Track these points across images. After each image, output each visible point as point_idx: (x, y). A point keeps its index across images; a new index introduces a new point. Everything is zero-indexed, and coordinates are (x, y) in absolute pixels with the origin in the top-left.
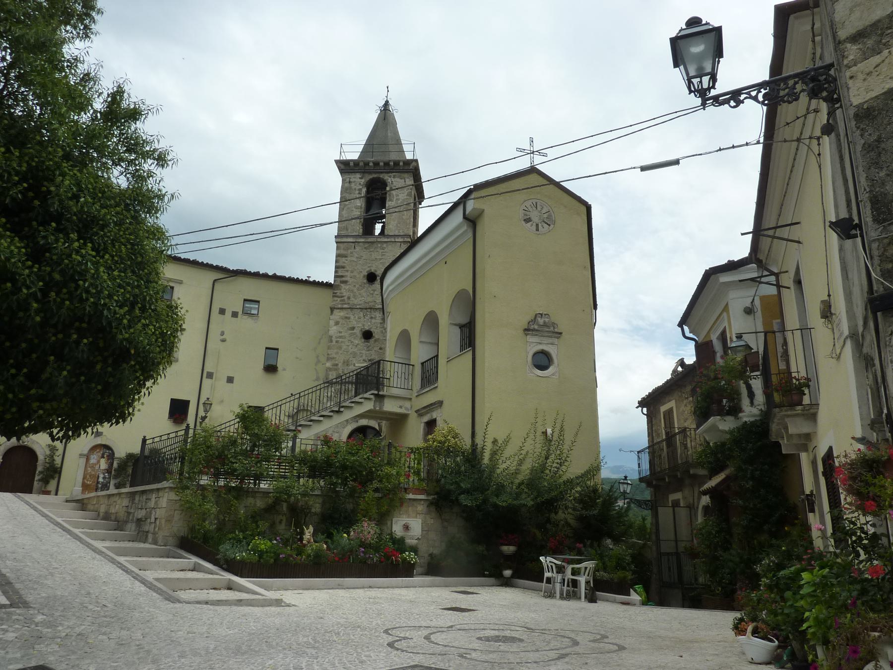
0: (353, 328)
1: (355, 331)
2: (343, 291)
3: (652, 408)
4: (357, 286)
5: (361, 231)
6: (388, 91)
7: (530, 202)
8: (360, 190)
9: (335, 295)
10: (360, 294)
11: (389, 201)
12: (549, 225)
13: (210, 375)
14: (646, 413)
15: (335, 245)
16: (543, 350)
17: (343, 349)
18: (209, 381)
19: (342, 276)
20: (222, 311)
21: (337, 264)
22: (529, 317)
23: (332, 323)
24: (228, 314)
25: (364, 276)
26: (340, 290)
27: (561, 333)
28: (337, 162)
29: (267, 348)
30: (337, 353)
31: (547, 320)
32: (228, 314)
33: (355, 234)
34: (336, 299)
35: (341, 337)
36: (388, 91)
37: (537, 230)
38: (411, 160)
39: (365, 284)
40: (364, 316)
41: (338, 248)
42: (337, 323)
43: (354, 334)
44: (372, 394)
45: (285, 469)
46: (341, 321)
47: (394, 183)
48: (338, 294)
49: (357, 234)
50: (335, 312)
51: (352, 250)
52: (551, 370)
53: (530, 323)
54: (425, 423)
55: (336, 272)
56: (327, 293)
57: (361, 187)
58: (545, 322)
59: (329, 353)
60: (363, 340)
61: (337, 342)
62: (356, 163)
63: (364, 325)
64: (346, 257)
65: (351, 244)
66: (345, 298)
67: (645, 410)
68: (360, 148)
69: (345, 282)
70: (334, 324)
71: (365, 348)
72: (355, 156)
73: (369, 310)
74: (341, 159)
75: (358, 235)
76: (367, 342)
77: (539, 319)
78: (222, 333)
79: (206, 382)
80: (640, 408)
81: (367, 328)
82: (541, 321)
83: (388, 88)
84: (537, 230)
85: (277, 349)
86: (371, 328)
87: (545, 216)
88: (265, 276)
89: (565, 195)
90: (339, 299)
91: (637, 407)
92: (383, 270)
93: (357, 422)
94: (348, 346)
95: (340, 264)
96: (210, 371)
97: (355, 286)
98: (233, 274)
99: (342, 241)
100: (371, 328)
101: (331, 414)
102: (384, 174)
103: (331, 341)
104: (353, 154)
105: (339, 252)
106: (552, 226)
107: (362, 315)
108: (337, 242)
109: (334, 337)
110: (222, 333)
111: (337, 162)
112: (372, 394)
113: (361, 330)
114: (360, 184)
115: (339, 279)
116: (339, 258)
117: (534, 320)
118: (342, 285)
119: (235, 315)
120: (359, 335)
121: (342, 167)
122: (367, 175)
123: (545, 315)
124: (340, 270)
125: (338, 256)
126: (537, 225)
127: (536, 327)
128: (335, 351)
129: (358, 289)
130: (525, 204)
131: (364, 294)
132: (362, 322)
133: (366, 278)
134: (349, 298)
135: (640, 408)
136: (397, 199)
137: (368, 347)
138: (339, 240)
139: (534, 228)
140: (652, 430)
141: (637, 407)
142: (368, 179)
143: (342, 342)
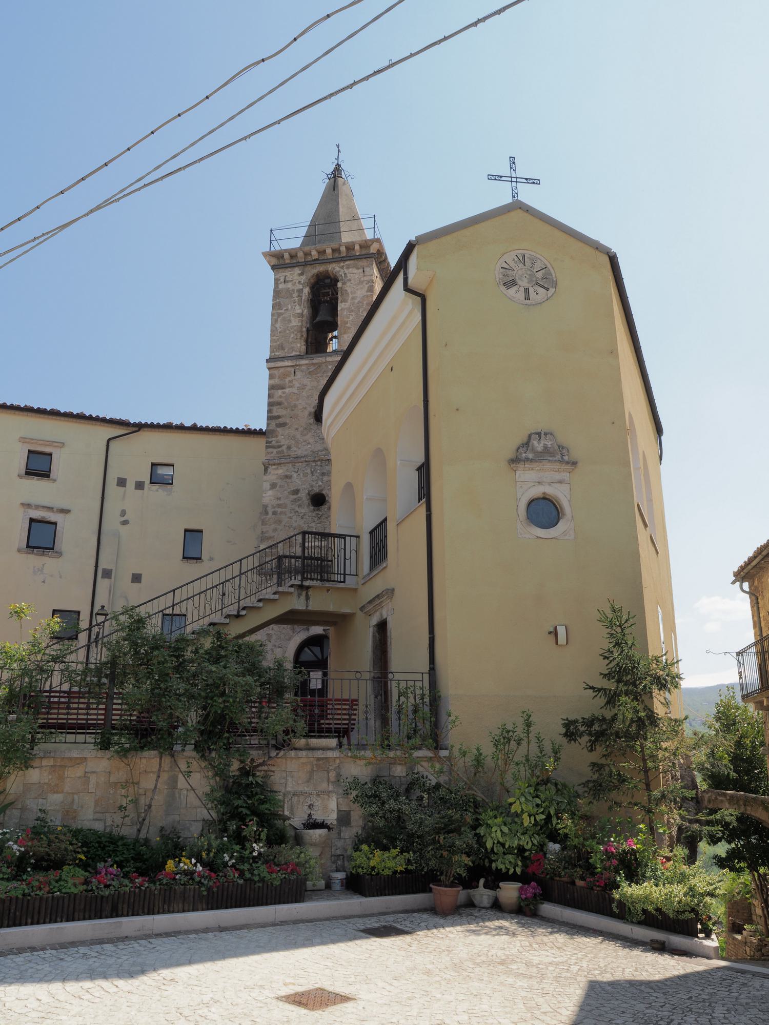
0: (296, 492)
1: (299, 495)
2: (280, 438)
3: (756, 583)
4: (301, 429)
5: (304, 347)
6: (339, 151)
7: (513, 254)
8: (300, 291)
9: (269, 446)
10: (305, 441)
11: (341, 302)
12: (547, 289)
13: (107, 574)
14: (748, 590)
15: (267, 372)
16: (544, 493)
17: (283, 523)
18: (106, 581)
19: (279, 417)
20: (122, 482)
21: (271, 400)
22: (521, 438)
23: (267, 486)
24: (131, 485)
25: (310, 415)
26: (277, 436)
27: (574, 464)
28: (265, 254)
29: (186, 531)
30: (275, 530)
31: (549, 444)
32: (131, 485)
33: (294, 353)
34: (270, 450)
35: (279, 506)
36: (339, 151)
37: (527, 298)
38: (371, 240)
39: (311, 424)
40: (312, 472)
41: (271, 377)
42: (273, 486)
43: (299, 499)
44: (292, 586)
45: (97, 714)
46: (279, 482)
47: (348, 275)
48: (273, 443)
49: (298, 353)
50: (271, 469)
51: (292, 377)
52: (562, 526)
53: (521, 450)
54: (374, 626)
55: (269, 411)
56: (259, 443)
57: (301, 287)
58: (545, 447)
59: (264, 530)
60: (312, 508)
61: (274, 513)
62: (293, 254)
63: (312, 486)
64: (283, 388)
65: (289, 369)
66: (284, 448)
67: (746, 586)
68: (303, 232)
69: (283, 425)
70: (269, 487)
71: (316, 519)
72: (296, 244)
73: (319, 463)
74: (273, 249)
75: (300, 355)
76: (318, 510)
77: (535, 443)
78: (123, 513)
79: (103, 584)
80: (738, 584)
81: (316, 490)
82: (538, 446)
83: (338, 146)
84: (527, 298)
85: (201, 531)
86: (322, 490)
87: (540, 274)
88: (181, 428)
89: (572, 240)
90: (275, 451)
91: (734, 583)
92: (317, 397)
93: (308, 630)
94: (290, 518)
95: (276, 399)
96: (105, 567)
97: (297, 429)
98: (135, 429)
99: (277, 365)
100: (322, 490)
101: (227, 621)
102: (334, 265)
103: (267, 513)
104: (292, 240)
105: (273, 382)
106: (552, 290)
107: (309, 471)
108: (269, 369)
109: (270, 506)
110: (123, 513)
111: (265, 254)
112: (292, 586)
113: (309, 494)
114: (300, 282)
115: (273, 423)
116: (272, 391)
117: (526, 444)
118: (278, 429)
119: (140, 486)
120: (306, 500)
121: (274, 261)
122: (308, 268)
123: (546, 434)
124: (275, 408)
125: (272, 388)
126: (527, 291)
127: (531, 456)
128: (273, 526)
129: (303, 435)
130: (505, 258)
131: (311, 440)
132: (305, 483)
133: (313, 416)
134: (289, 448)
135: (738, 584)
136: (353, 298)
137: (319, 518)
138: (272, 365)
139: (521, 295)
140: (759, 618)
141: (734, 583)
142: (310, 275)
143: (281, 513)
